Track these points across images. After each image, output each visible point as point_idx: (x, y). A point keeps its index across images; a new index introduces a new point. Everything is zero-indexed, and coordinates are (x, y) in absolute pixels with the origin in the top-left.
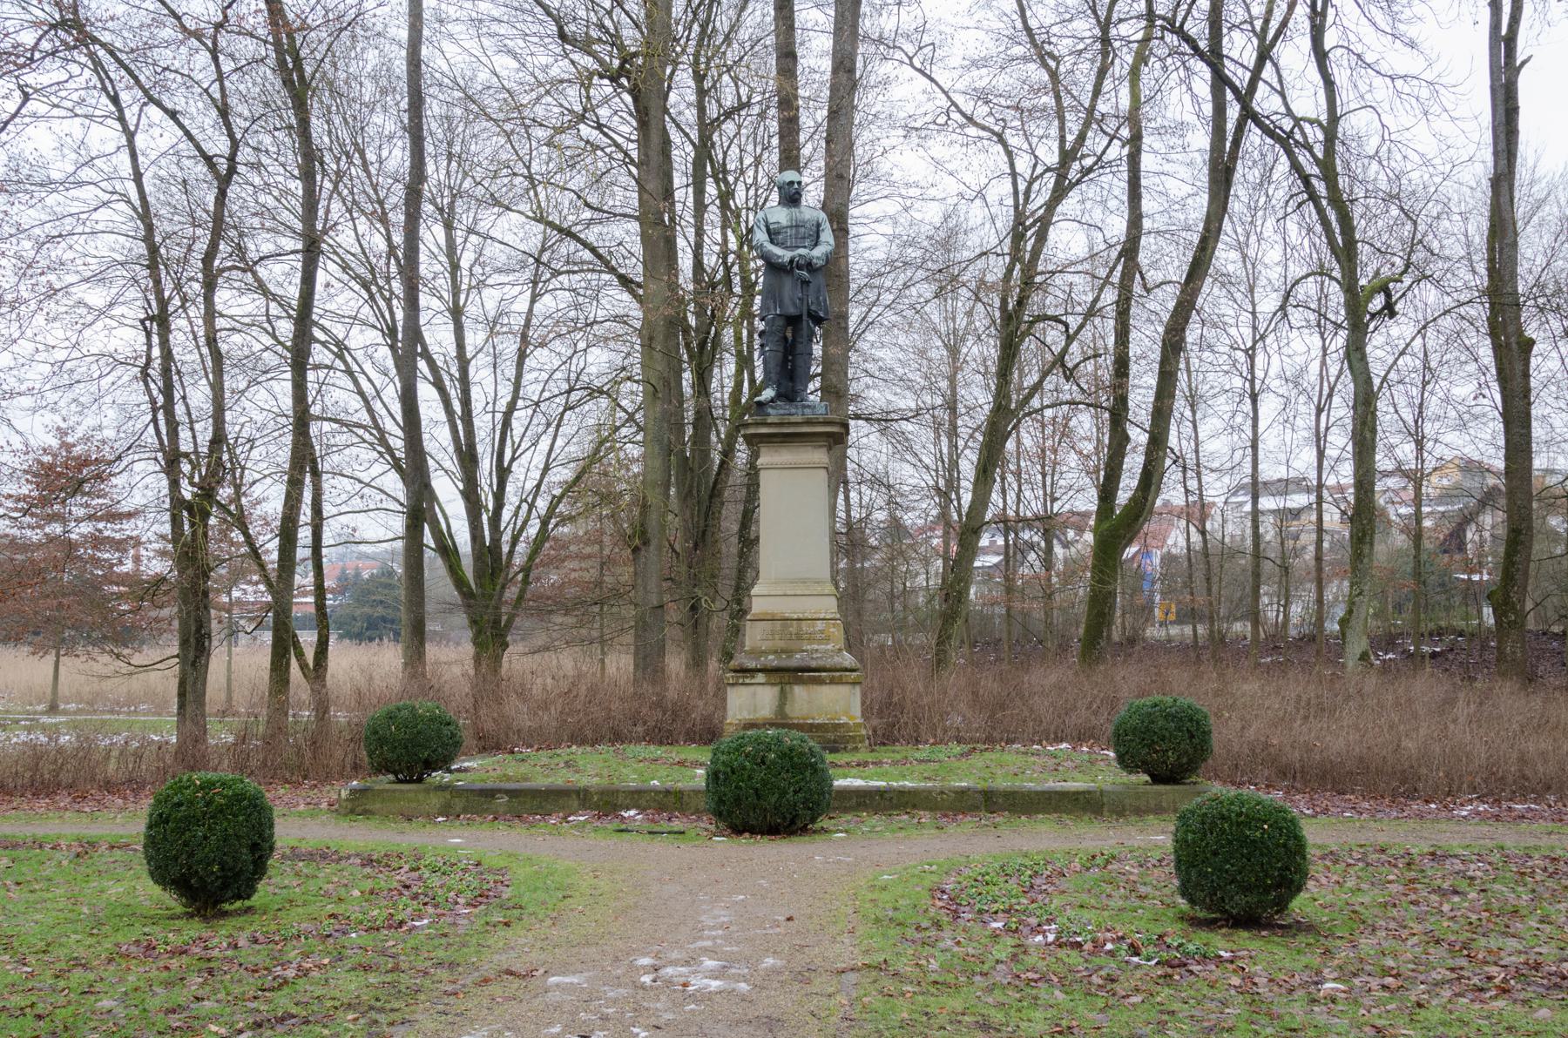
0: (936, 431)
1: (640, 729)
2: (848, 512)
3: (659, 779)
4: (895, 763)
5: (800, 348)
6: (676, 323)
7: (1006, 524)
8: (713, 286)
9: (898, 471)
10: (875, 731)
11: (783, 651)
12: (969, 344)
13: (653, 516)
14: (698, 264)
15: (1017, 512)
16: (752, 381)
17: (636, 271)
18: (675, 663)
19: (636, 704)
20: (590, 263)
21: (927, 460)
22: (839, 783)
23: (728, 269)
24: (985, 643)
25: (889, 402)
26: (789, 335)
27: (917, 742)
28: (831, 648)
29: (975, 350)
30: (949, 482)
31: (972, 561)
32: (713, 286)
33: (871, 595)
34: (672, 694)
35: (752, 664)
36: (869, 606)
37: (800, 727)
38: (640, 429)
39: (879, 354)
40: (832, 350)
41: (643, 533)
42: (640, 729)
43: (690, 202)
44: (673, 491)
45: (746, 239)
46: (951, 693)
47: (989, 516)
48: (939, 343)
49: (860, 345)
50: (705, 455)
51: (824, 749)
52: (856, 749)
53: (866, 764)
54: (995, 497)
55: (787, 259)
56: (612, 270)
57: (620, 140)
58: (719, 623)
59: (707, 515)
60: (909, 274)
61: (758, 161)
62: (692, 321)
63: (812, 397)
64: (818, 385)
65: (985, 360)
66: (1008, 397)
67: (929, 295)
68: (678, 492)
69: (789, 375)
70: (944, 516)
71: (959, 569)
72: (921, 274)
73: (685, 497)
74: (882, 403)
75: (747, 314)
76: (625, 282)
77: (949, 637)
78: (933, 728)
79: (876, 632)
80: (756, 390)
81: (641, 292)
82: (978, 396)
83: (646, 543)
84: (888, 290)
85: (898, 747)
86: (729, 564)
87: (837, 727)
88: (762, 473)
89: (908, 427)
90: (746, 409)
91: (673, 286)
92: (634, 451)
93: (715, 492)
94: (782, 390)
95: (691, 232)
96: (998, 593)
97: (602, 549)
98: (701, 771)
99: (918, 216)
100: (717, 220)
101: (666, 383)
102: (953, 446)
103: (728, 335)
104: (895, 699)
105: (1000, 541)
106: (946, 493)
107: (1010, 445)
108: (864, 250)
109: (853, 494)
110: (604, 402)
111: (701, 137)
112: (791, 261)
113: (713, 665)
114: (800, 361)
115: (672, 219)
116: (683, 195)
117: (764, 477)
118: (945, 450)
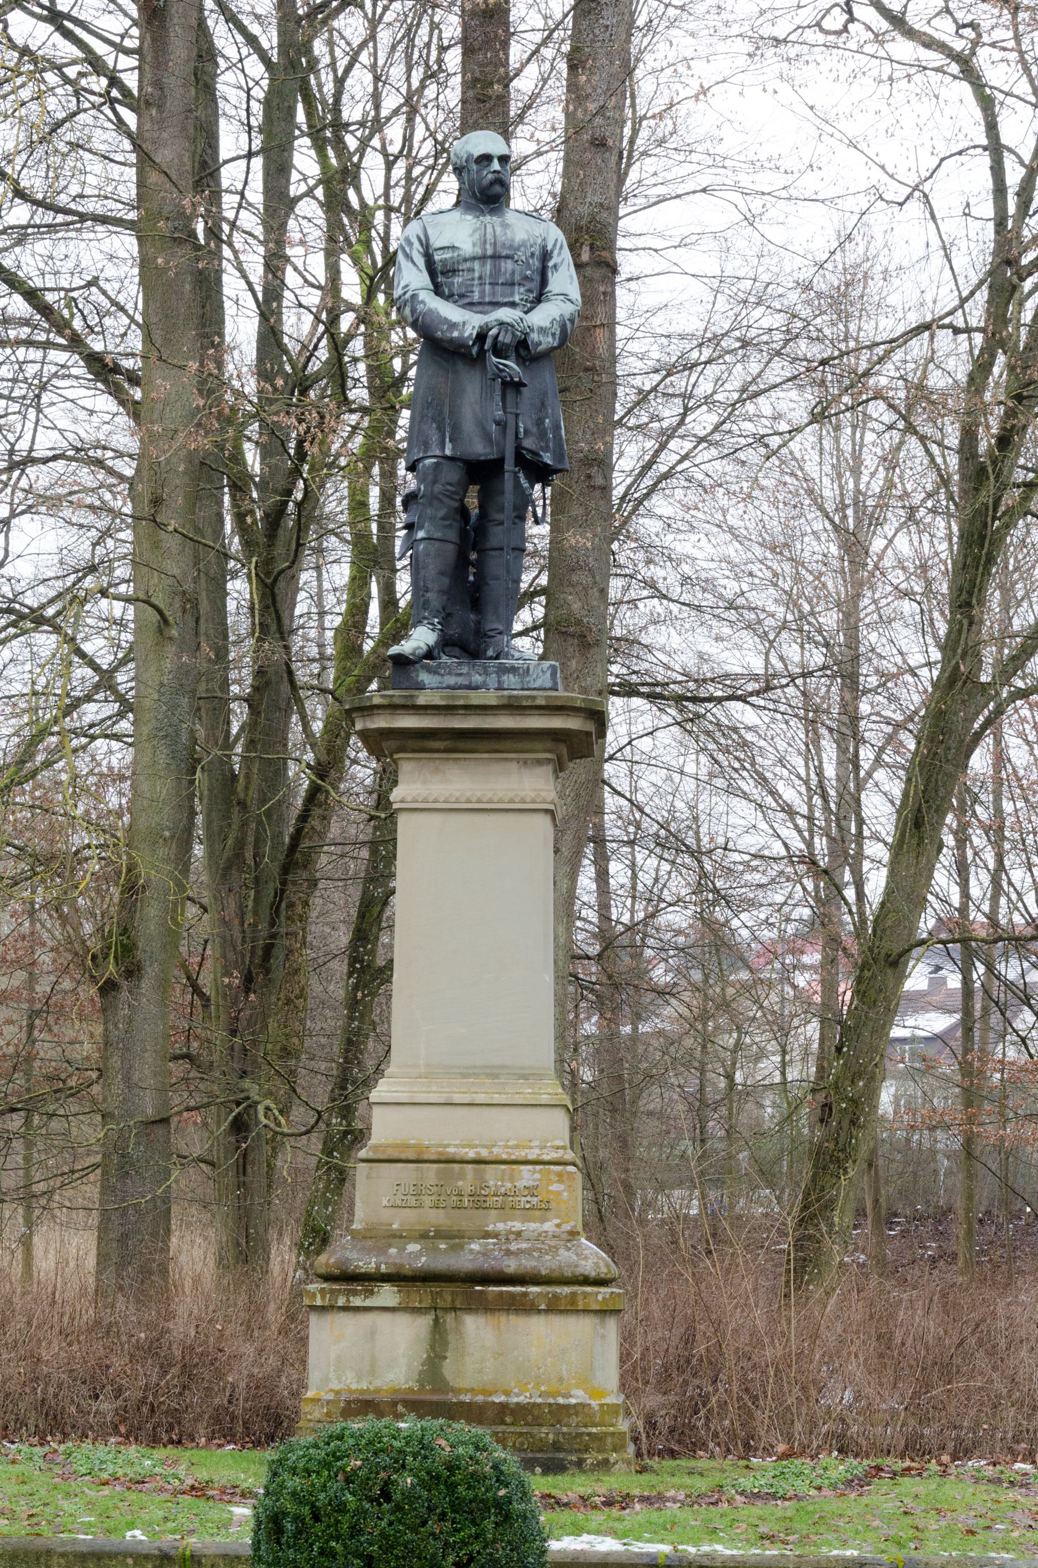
0: (811, 725)
1: (106, 1406)
2: (603, 909)
3: (147, 1527)
4: (693, 1500)
5: (497, 535)
6: (216, 469)
7: (963, 942)
8: (302, 384)
9: (721, 806)
10: (651, 1424)
11: (441, 1234)
12: (889, 529)
13: (151, 915)
14: (270, 335)
15: (992, 918)
16: (389, 602)
17: (122, 339)
18: (194, 1251)
19: (98, 1348)
20: (26, 322)
21: (789, 794)
22: (561, 1545)
23: (338, 346)
24: (917, 1224)
25: (702, 657)
26: (472, 501)
27: (749, 1450)
28: (552, 1230)
29: (902, 543)
30: (839, 845)
31: (888, 1024)
32: (302, 384)
33: (652, 1099)
34: (181, 1329)
35: (367, 1264)
36: (649, 1127)
37: (474, 1413)
38: (126, 707)
39: (682, 545)
40: (574, 539)
41: (127, 949)
42: (106, 1406)
43: (256, 195)
44: (198, 850)
45: (377, 279)
46: (829, 1339)
47: (927, 923)
48: (820, 524)
49: (646, 526)
50: (275, 772)
51: (529, 1464)
52: (604, 1465)
53: (625, 1501)
54: (943, 880)
55: (470, 332)
56: (76, 343)
57: (100, 48)
58: (298, 1159)
59: (275, 910)
60: (754, 368)
61: (411, 107)
62: (252, 457)
63: (523, 644)
64: (539, 612)
65: (924, 568)
66: (973, 654)
67: (800, 416)
68: (211, 853)
69: (469, 599)
70: (823, 921)
71: (856, 1041)
72: (779, 370)
73: (227, 866)
74: (687, 660)
75: (378, 451)
76: (103, 369)
77: (829, 1206)
78: (784, 1420)
79: (662, 1187)
80: (396, 627)
81: (137, 394)
82: (907, 646)
83: (133, 972)
84: (708, 400)
85: (703, 1463)
86: (324, 1024)
87: (560, 1412)
88: (402, 820)
89: (742, 714)
90: (373, 669)
91: (211, 384)
92: (113, 755)
93: (296, 858)
94: (454, 631)
95: (255, 263)
96: (945, 1100)
97: (32, 979)
98: (243, 1511)
99: (776, 234)
100: (316, 235)
101: (190, 603)
102: (850, 762)
103: (335, 501)
104: (701, 1349)
105: (954, 981)
106: (827, 872)
107: (980, 761)
108: (653, 312)
109: (614, 867)
110: (46, 642)
111: (284, 46)
112: (481, 337)
113: (283, 1258)
114: (495, 565)
115: (213, 233)
116: (241, 176)
117: (405, 825)
118: (830, 771)
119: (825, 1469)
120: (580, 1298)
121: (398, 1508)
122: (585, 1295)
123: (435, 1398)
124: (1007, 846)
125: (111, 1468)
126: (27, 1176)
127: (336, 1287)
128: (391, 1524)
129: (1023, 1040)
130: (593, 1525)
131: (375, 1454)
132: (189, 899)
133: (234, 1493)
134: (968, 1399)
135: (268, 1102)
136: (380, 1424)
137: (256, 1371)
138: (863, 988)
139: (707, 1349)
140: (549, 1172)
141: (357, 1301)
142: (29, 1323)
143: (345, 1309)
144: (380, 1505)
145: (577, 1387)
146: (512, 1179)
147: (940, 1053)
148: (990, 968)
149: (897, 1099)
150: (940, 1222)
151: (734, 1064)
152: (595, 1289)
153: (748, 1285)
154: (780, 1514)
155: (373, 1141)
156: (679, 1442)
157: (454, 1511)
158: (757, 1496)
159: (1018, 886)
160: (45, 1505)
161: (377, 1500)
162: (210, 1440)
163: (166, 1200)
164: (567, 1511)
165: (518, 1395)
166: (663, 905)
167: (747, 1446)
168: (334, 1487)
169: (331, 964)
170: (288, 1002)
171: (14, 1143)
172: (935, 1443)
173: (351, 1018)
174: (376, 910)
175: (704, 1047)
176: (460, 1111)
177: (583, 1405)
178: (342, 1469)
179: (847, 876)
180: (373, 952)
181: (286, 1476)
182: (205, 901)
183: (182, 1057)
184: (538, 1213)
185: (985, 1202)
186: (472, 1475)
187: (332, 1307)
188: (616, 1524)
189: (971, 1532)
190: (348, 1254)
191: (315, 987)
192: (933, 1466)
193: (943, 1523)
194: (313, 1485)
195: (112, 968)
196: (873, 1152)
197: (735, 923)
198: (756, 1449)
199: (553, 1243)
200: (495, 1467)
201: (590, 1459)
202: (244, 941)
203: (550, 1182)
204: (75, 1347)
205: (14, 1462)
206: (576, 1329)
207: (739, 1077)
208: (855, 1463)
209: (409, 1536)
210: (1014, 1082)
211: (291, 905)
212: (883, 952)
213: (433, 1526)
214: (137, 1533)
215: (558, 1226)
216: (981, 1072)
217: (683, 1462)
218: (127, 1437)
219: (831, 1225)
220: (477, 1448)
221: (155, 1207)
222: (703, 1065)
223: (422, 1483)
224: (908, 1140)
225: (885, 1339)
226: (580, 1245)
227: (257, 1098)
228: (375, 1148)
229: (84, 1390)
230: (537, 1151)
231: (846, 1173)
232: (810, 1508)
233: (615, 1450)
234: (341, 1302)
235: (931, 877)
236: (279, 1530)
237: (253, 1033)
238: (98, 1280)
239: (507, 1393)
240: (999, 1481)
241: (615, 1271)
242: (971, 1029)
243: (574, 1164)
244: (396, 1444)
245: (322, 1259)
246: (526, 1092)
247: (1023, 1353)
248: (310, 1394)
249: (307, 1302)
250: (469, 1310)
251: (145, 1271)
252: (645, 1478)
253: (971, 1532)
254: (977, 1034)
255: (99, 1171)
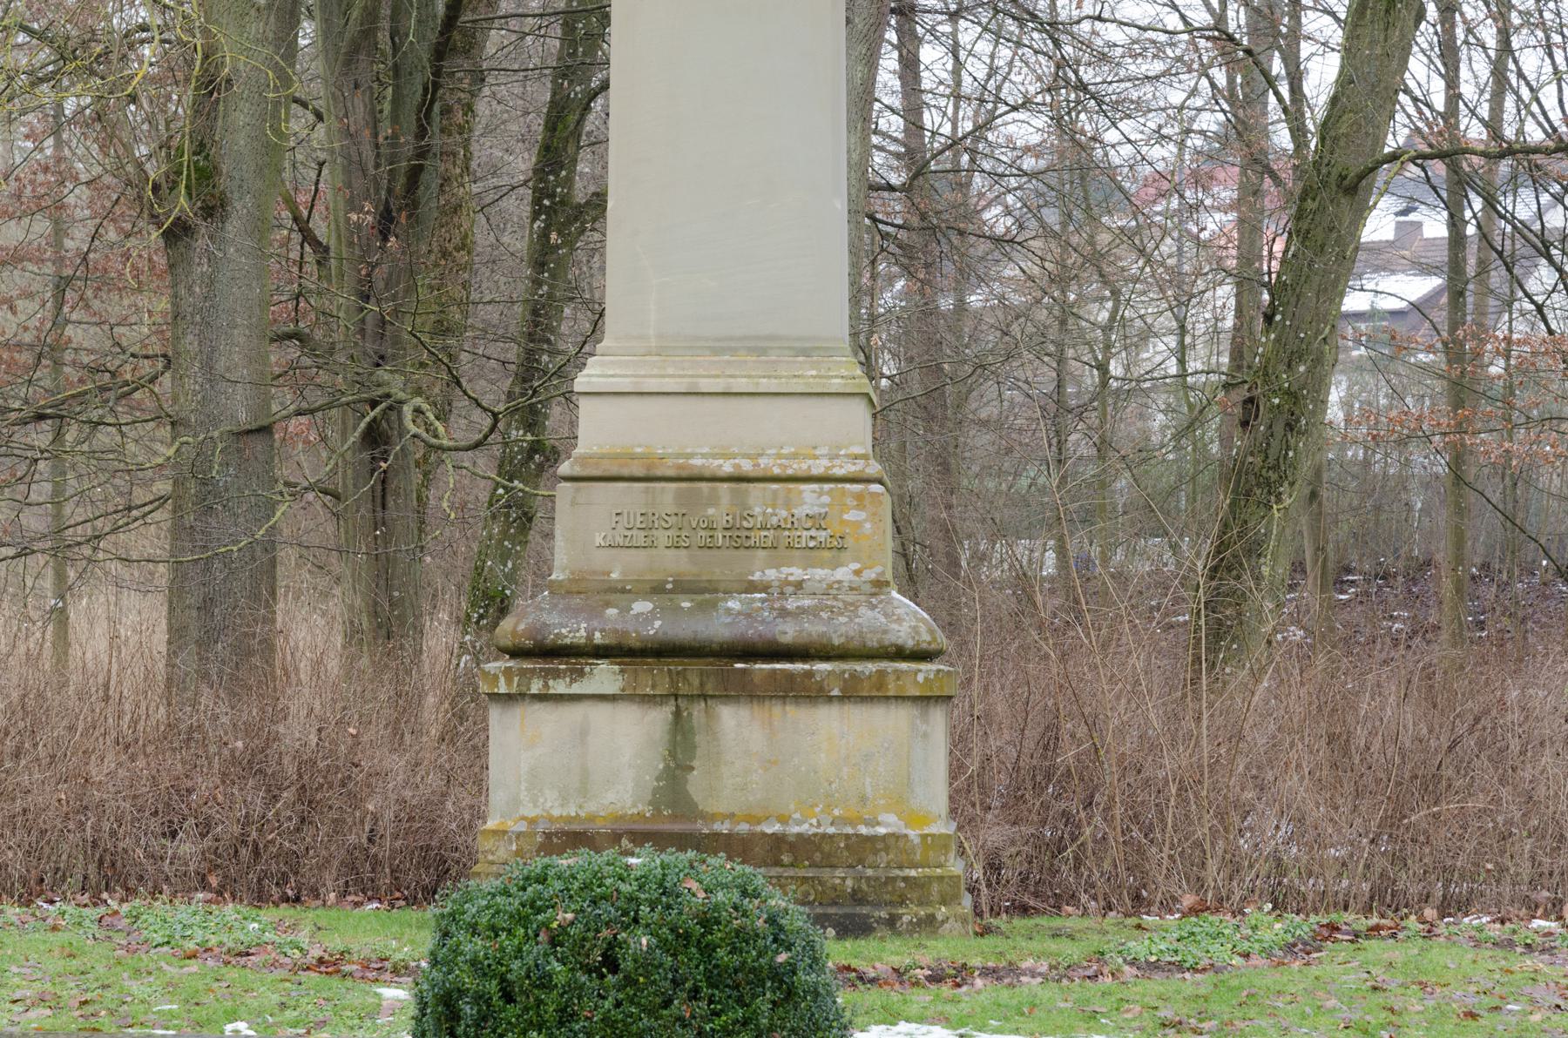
2: (912, 112)
4: (1061, 973)
7: (1453, 166)
10: (994, 866)
11: (684, 587)
13: (239, 124)
18: (311, 628)
19: (175, 764)
27: (1139, 902)
28: (846, 580)
33: (987, 402)
35: (574, 631)
37: (738, 847)
41: (206, 175)
42: (187, 847)
46: (1259, 739)
47: (1397, 137)
52: (929, 924)
53: (960, 975)
54: (1420, 71)
58: (462, 486)
70: (1243, 130)
77: (1255, 550)
83: (214, 209)
85: (1071, 920)
86: (498, 287)
96: (1425, 402)
97: (59, 231)
98: (397, 994)
105: (1435, 226)
113: (440, 636)
119: (1255, 928)
120: (891, 678)
121: (629, 981)
122: (899, 674)
123: (677, 827)
124: (1516, 19)
125: (199, 935)
126: (58, 516)
127: (527, 665)
128: (618, 1004)
129: (1539, 308)
130: (914, 1009)
131: (594, 902)
132: (296, 101)
133: (383, 968)
134: (1464, 827)
135: (418, 401)
136: (600, 860)
137: (408, 793)
138: (1304, 225)
139: (1077, 757)
140: (843, 492)
141: (559, 687)
142: (71, 728)
143: (542, 698)
144: (602, 977)
145: (887, 809)
146: (788, 504)
147: (1415, 328)
148: (1490, 202)
149: (1346, 404)
150: (1414, 581)
151: (1108, 347)
152: (913, 666)
153: (1137, 662)
154: (1189, 990)
155: (580, 449)
156: (1036, 895)
157: (711, 985)
158: (1155, 966)
159: (1531, 77)
160: (104, 987)
161: (597, 970)
162: (343, 894)
163: (270, 546)
164: (875, 990)
165: (799, 823)
166: (1003, 108)
167: (1137, 898)
168: (534, 951)
169: (503, 204)
170: (445, 254)
171: (42, 465)
172: (1415, 889)
173: (538, 283)
174: (572, 119)
175: (1063, 323)
176: (708, 403)
177: (896, 837)
178: (545, 925)
179: (1277, 66)
180: (569, 182)
181: (462, 936)
182: (320, 104)
183: (289, 336)
184: (827, 554)
185: (1481, 549)
186: (737, 932)
187: (522, 696)
188: (948, 1008)
189: (1472, 1015)
190: (545, 617)
191: (482, 237)
192: (1412, 921)
193: (1431, 1003)
194: (502, 949)
195: (183, 203)
196: (1318, 473)
197: (1111, 136)
198: (1150, 904)
199: (849, 599)
200: (772, 921)
201: (907, 915)
202: (377, 166)
203: (844, 508)
204: (141, 763)
205: (55, 928)
206: (885, 725)
207: (1115, 368)
208: (1298, 919)
209: (646, 1021)
210: (1522, 373)
211: (447, 111)
212: (1335, 172)
213: (680, 1007)
214: (242, 1026)
215: (857, 573)
216: (1478, 355)
217: (1042, 921)
218: (219, 893)
219: (1258, 578)
220: (744, 893)
221: (253, 559)
222: (1061, 347)
223: (663, 944)
224: (1366, 463)
225: (1338, 742)
226: (890, 601)
227: (401, 396)
228: (583, 460)
229: (154, 825)
230: (825, 462)
231: (1279, 500)
232: (1235, 982)
233: (944, 902)
234: (536, 687)
235: (1403, 66)
236: (454, 1016)
237: (394, 297)
238: (170, 665)
239: (784, 820)
240: (1510, 944)
241: (942, 640)
242: (1461, 294)
243: (880, 482)
244: (625, 888)
245: (507, 624)
246: (808, 375)
247: (1547, 759)
248: (491, 824)
249: (484, 688)
250: (726, 698)
251: (243, 653)
252: (988, 942)
253: (1472, 1015)
254: (1470, 299)
255: (169, 505)
